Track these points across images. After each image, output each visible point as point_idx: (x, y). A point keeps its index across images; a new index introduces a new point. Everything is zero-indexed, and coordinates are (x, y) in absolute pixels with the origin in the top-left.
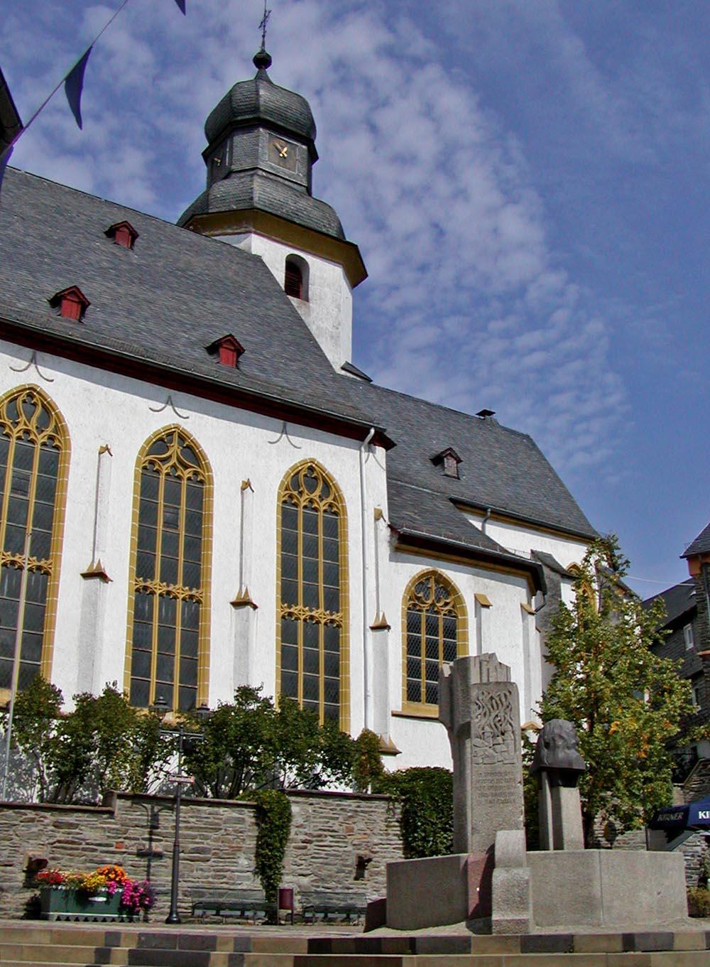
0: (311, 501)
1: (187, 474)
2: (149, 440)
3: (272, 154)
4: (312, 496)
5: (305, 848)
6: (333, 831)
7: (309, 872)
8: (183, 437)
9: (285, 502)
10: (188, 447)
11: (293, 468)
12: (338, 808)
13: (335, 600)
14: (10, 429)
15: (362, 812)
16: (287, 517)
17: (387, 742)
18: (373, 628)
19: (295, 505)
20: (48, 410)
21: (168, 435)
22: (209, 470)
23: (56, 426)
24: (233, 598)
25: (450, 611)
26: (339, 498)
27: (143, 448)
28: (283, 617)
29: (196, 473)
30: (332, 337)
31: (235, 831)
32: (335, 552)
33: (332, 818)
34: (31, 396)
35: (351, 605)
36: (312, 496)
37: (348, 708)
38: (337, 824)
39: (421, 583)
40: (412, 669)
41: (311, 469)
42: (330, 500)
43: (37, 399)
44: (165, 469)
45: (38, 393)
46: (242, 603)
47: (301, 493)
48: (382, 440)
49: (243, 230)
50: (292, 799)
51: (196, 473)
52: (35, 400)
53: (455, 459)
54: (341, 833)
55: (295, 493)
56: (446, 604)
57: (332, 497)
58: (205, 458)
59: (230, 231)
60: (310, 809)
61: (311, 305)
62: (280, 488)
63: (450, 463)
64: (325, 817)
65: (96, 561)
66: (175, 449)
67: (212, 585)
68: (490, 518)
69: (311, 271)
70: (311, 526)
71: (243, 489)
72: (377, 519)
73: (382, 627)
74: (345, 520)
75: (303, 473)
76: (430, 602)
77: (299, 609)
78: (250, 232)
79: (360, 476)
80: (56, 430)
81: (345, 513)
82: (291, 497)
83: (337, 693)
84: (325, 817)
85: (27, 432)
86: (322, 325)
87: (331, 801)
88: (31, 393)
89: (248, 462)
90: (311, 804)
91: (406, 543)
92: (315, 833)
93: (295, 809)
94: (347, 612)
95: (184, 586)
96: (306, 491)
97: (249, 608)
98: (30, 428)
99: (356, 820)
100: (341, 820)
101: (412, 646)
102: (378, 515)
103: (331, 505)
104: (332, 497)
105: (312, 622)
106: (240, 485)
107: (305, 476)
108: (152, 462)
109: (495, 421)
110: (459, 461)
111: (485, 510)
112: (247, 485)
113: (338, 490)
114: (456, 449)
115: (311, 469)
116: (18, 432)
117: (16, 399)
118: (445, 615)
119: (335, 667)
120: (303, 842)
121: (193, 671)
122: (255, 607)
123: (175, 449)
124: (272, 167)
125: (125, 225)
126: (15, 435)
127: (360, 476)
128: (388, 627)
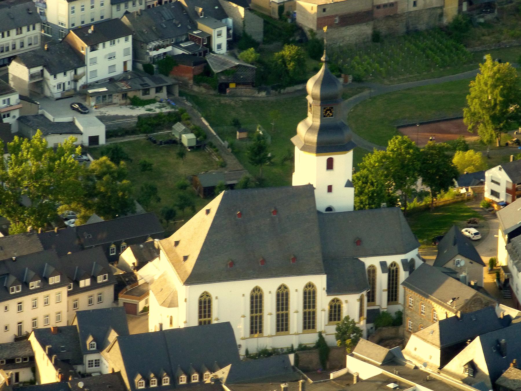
89: (296, 285)
123: (283, 287)
127: (320, 281)
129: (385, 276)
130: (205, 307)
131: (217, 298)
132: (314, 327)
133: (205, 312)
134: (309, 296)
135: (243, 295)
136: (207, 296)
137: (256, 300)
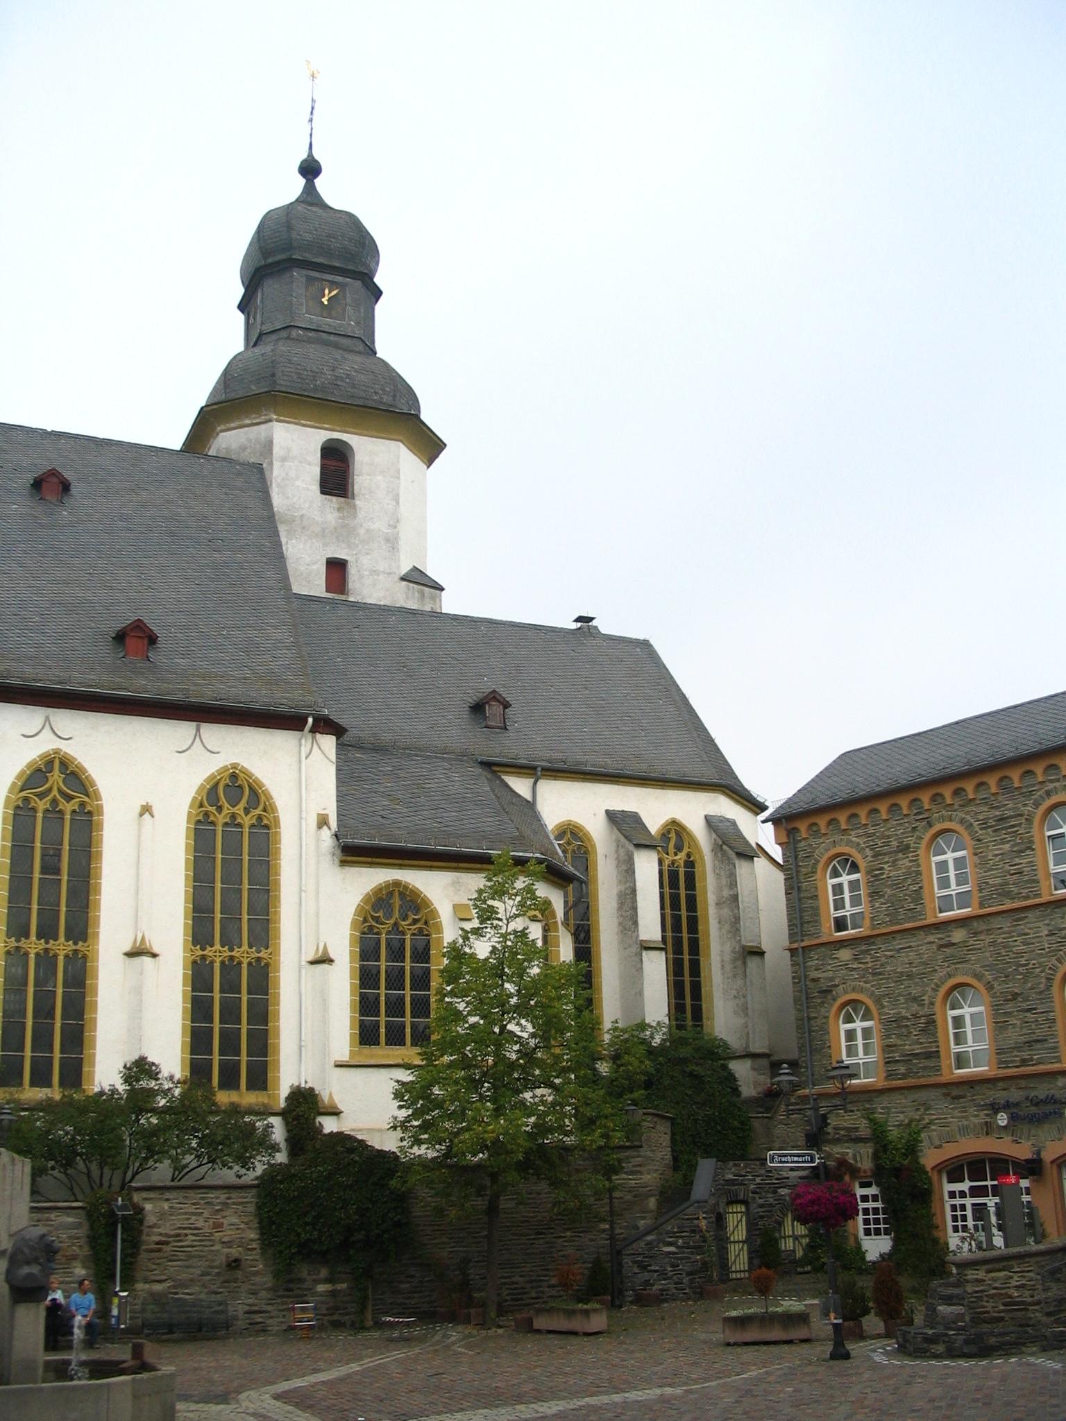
3: (311, 303)
4: (234, 810)
5: (159, 1250)
6: (196, 1229)
7: (163, 1277)
9: (199, 822)
11: (207, 780)
15: (234, 1204)
17: (326, 1099)
22: (97, 796)
24: (127, 947)
25: (421, 929)
26: (269, 808)
27: (14, 784)
28: (194, 962)
30: (388, 540)
31: (70, 1237)
33: (194, 1214)
35: (282, 938)
36: (234, 810)
37: (277, 1063)
38: (201, 1219)
39: (380, 904)
40: (366, 1006)
41: (234, 777)
42: (258, 811)
44: (42, 805)
46: (138, 952)
48: (325, 725)
49: (263, 418)
53: (501, 703)
54: (206, 1230)
56: (415, 921)
58: (93, 784)
59: (248, 422)
60: (166, 1206)
61: (357, 502)
63: (493, 710)
66: (56, 777)
67: (101, 936)
68: (544, 776)
69: (357, 457)
71: (141, 815)
72: (320, 827)
73: (324, 960)
76: (392, 921)
78: (271, 421)
79: (300, 779)
80: (265, 810)
81: (277, 824)
82: (207, 814)
83: (266, 1046)
86: (373, 527)
90: (167, 1200)
91: (353, 853)
92: (173, 1233)
93: (148, 1207)
94: (277, 952)
95: (67, 940)
96: (226, 805)
97: (147, 960)
99: (225, 1214)
100: (206, 1214)
101: (366, 978)
102: (323, 822)
106: (138, 810)
108: (26, 799)
109: (596, 628)
110: (506, 705)
111: (534, 768)
112: (146, 810)
113: (269, 797)
114: (501, 691)
115: (234, 777)
118: (413, 934)
119: (263, 1013)
120: (157, 1243)
121: (77, 1037)
122: (154, 956)
123: (56, 777)
124: (311, 321)
125: (53, 473)
127: (300, 779)
128: (331, 961)
129: (647, 868)
134: (231, 841)
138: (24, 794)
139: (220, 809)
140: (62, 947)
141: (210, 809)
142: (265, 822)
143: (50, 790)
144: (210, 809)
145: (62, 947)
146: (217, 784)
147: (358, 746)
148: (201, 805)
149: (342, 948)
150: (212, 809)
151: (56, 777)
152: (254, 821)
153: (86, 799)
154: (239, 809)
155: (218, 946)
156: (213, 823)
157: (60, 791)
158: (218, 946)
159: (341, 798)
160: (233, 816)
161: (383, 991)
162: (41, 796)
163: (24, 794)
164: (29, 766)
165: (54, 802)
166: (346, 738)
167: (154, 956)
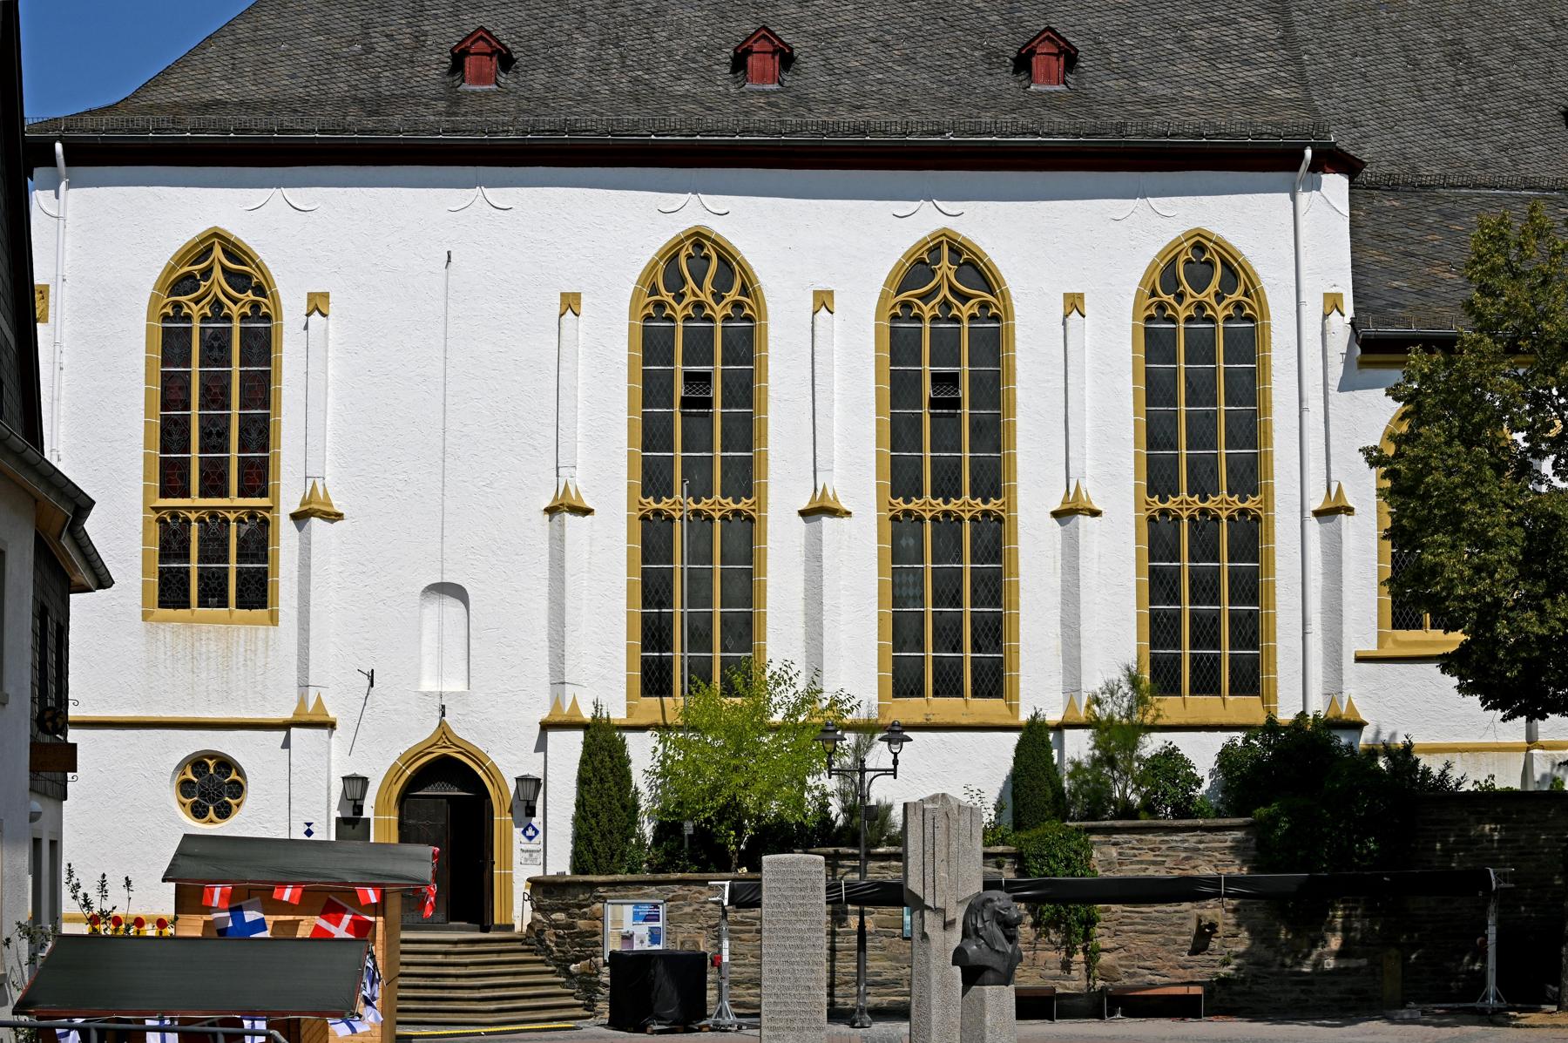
0: (1200, 306)
1: (966, 310)
2: (899, 265)
8: (235, 251)
9: (1149, 319)
10: (968, 262)
12: (1164, 847)
13: (1250, 476)
14: (1213, 309)
16: (1155, 343)
18: (1317, 514)
19: (1172, 320)
20: (1233, 272)
21: (930, 251)
23: (743, 285)
28: (1151, 519)
29: (984, 306)
32: (1248, 389)
34: (699, 246)
36: (1200, 297)
41: (1199, 248)
42: (1237, 296)
43: (709, 250)
44: (928, 311)
45: (714, 241)
47: (1180, 297)
48: (1332, 159)
50: (1094, 838)
51: (984, 306)
52: (1207, 255)
55: (1170, 299)
57: (1241, 289)
60: (1114, 852)
62: (159, 286)
64: (1141, 862)
65: (820, 488)
66: (945, 268)
70: (1201, 349)
74: (1011, 329)
75: (1182, 258)
77: (1184, 503)
79: (1297, 245)
80: (744, 291)
81: (1264, 313)
84: (1141, 862)
85: (699, 306)
87: (1150, 837)
88: (698, 238)
89: (1072, 269)
90: (1115, 844)
98: (702, 297)
102: (1332, 303)
103: (738, 305)
104: (1241, 289)
105: (948, 525)
107: (1188, 262)
108: (906, 305)
116: (1226, 307)
117: (677, 255)
122: (1095, 513)
123: (945, 268)
126: (679, 316)
127: (1297, 245)
130: (215, 394)
131: (318, 304)
132: (992, 681)
133: (214, 436)
135: (570, 302)
136: (241, 281)
137: (697, 370)
138: (901, 297)
139: (1180, 297)
140: (966, 505)
141: (1165, 298)
142: (264, 310)
143: (937, 289)
144: (1165, 298)
145: (966, 505)
146: (1175, 258)
147: (1391, 186)
148: (1154, 294)
149: (1364, 489)
150: (1170, 299)
151: (945, 269)
152: (1231, 311)
153: (990, 298)
154: (1208, 296)
155: (1184, 495)
156: (1211, 320)
157: (952, 289)
158: (1184, 495)
159: (1358, 269)
160: (1200, 306)
161: (678, 453)
162: (925, 298)
163: (901, 297)
164: (907, 256)
165: (946, 304)
166: (1367, 174)
167: (1095, 513)
